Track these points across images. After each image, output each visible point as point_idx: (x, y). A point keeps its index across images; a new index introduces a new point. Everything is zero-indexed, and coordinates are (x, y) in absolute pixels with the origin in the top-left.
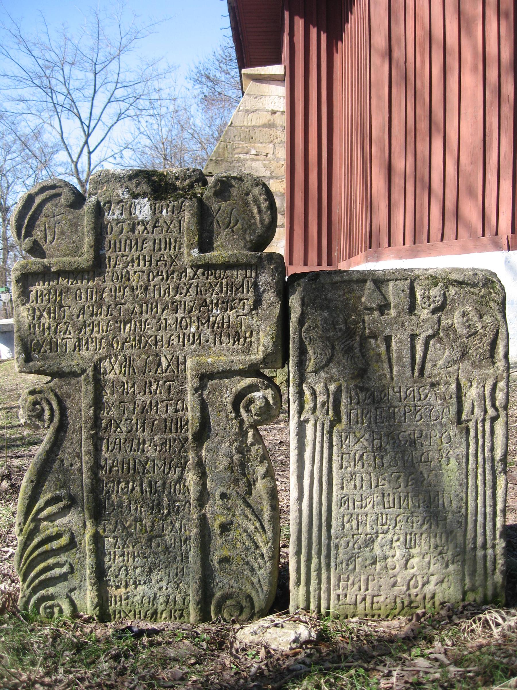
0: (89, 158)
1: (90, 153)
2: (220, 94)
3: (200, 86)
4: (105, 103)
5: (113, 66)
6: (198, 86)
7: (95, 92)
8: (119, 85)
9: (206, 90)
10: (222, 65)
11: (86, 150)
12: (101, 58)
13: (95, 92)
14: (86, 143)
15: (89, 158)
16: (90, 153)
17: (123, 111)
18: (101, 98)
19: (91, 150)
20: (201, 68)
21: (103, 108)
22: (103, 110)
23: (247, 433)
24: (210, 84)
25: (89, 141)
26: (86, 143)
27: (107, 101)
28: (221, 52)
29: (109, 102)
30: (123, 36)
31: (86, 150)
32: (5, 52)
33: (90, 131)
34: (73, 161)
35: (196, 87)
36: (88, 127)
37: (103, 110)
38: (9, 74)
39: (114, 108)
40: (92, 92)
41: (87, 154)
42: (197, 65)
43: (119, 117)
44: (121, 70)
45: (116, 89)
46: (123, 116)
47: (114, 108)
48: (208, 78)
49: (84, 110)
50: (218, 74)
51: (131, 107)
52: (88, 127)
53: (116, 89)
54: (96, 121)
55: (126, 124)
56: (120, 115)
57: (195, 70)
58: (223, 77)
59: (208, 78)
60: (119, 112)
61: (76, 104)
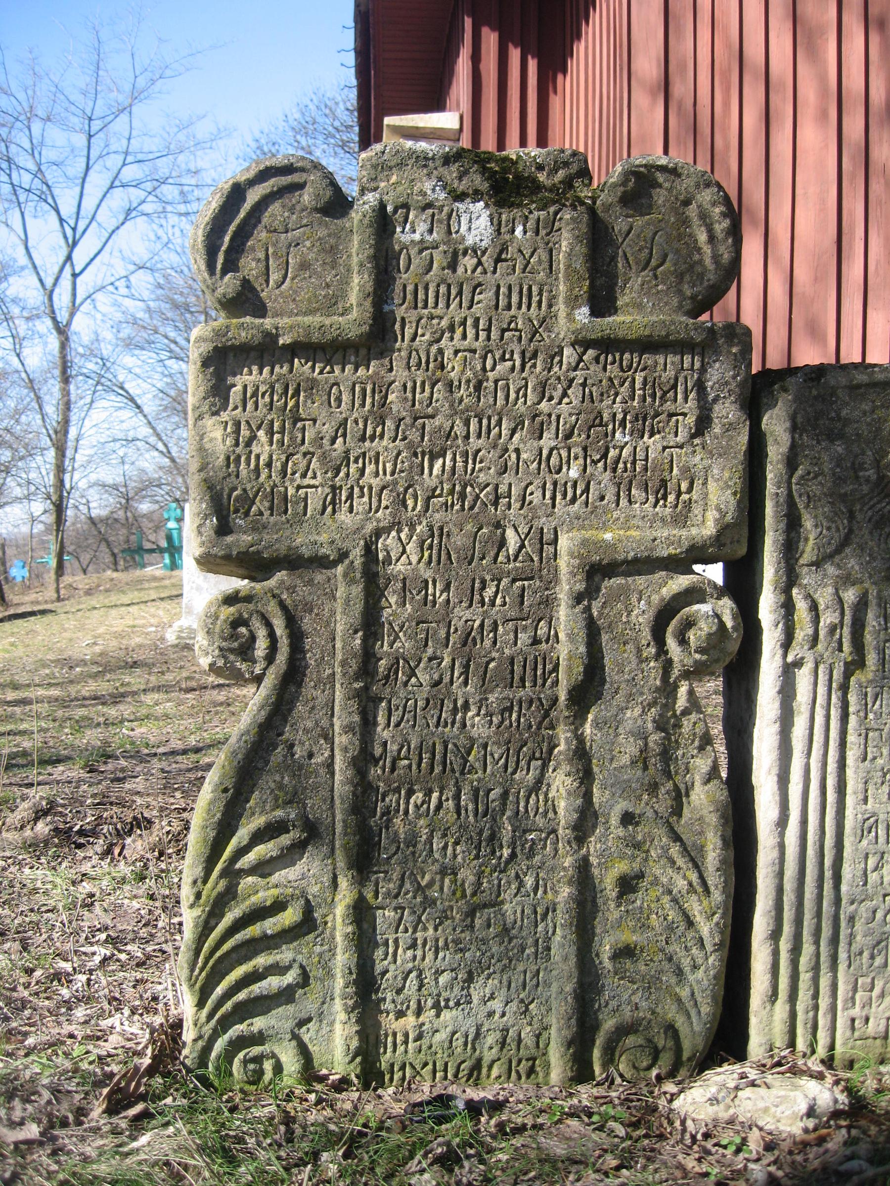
1: (75, 276)
4: (105, 190)
5: (120, 124)
8: (130, 159)
10: (298, 137)
14: (69, 258)
16: (75, 276)
17: (135, 205)
18: (98, 181)
19: (77, 271)
21: (100, 197)
22: (101, 201)
25: (75, 255)
26: (69, 258)
28: (298, 116)
29: (112, 187)
30: (138, 73)
33: (77, 237)
36: (74, 229)
37: (101, 201)
39: (118, 200)
41: (69, 277)
42: (258, 135)
44: (134, 133)
45: (124, 164)
46: (134, 214)
51: (151, 198)
52: (74, 229)
53: (124, 164)
55: (139, 226)
56: (129, 211)
57: (254, 145)
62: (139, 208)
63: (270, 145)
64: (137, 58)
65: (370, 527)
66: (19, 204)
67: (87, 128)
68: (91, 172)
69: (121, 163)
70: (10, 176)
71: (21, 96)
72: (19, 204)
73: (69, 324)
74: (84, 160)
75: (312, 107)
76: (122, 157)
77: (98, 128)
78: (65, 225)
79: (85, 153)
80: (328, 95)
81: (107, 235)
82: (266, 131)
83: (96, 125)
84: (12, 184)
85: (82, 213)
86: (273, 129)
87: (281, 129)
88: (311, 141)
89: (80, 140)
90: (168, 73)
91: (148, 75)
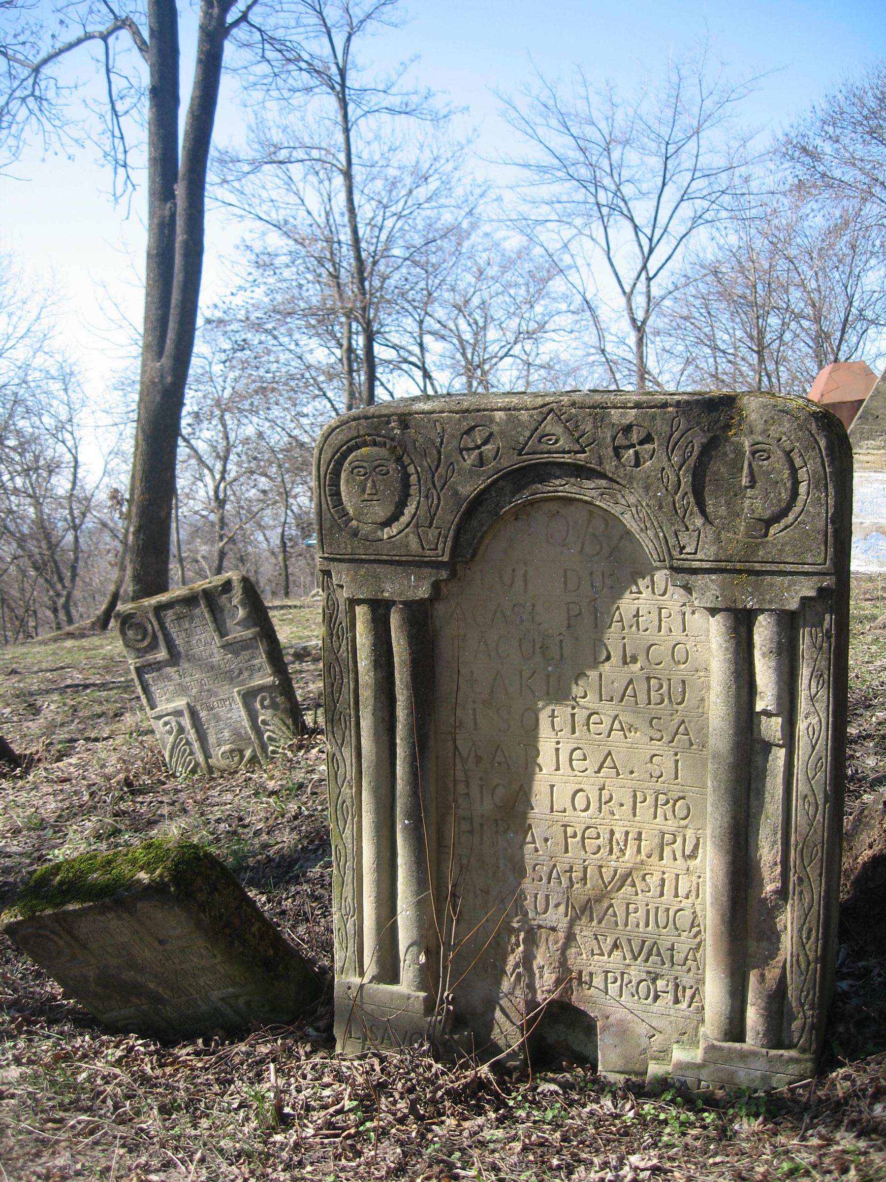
0: (648, 286)
1: (649, 279)
2: (824, 175)
3: (791, 164)
5: (691, 146)
6: (787, 165)
7: (664, 184)
8: (697, 174)
9: (800, 170)
10: (826, 127)
11: (643, 275)
12: (678, 135)
13: (664, 184)
14: (644, 267)
15: (648, 286)
16: (649, 279)
17: (699, 214)
18: (671, 193)
19: (651, 275)
20: (793, 135)
23: (771, 912)
24: (807, 160)
27: (678, 198)
28: (825, 106)
29: (682, 200)
30: (704, 97)
31: (643, 275)
32: (530, 131)
34: (624, 292)
35: (784, 166)
36: (651, 240)
38: (531, 163)
39: (686, 210)
40: (660, 184)
42: (788, 129)
43: (697, 220)
44: (701, 151)
45: (693, 179)
47: (686, 210)
48: (804, 150)
49: (642, 212)
50: (818, 142)
52: (651, 240)
53: (693, 179)
54: (662, 231)
55: (702, 233)
57: (783, 139)
58: (828, 148)
59: (804, 150)
60: (692, 215)
61: (630, 205)
62: (704, 216)
63: (799, 138)
64: (704, 84)
65: (212, 493)
66: (602, 217)
67: (664, 151)
68: (666, 188)
69: (690, 178)
70: (596, 196)
71: (603, 125)
72: (602, 217)
73: (644, 322)
74: (661, 179)
75: (839, 96)
76: (691, 174)
77: (673, 150)
78: (640, 234)
79: (662, 173)
80: (858, 84)
81: (676, 243)
82: (795, 125)
83: (672, 149)
84: (268, 61)
85: (658, 224)
86: (801, 122)
87: (809, 119)
88: (838, 131)
89: (656, 163)
90: (734, 96)
91: (716, 98)
